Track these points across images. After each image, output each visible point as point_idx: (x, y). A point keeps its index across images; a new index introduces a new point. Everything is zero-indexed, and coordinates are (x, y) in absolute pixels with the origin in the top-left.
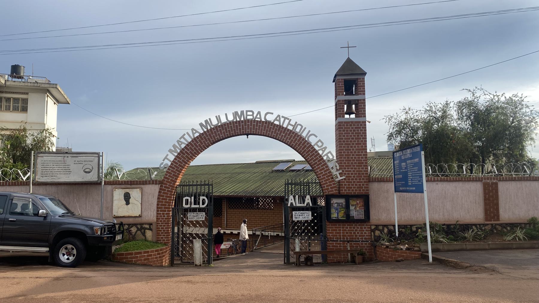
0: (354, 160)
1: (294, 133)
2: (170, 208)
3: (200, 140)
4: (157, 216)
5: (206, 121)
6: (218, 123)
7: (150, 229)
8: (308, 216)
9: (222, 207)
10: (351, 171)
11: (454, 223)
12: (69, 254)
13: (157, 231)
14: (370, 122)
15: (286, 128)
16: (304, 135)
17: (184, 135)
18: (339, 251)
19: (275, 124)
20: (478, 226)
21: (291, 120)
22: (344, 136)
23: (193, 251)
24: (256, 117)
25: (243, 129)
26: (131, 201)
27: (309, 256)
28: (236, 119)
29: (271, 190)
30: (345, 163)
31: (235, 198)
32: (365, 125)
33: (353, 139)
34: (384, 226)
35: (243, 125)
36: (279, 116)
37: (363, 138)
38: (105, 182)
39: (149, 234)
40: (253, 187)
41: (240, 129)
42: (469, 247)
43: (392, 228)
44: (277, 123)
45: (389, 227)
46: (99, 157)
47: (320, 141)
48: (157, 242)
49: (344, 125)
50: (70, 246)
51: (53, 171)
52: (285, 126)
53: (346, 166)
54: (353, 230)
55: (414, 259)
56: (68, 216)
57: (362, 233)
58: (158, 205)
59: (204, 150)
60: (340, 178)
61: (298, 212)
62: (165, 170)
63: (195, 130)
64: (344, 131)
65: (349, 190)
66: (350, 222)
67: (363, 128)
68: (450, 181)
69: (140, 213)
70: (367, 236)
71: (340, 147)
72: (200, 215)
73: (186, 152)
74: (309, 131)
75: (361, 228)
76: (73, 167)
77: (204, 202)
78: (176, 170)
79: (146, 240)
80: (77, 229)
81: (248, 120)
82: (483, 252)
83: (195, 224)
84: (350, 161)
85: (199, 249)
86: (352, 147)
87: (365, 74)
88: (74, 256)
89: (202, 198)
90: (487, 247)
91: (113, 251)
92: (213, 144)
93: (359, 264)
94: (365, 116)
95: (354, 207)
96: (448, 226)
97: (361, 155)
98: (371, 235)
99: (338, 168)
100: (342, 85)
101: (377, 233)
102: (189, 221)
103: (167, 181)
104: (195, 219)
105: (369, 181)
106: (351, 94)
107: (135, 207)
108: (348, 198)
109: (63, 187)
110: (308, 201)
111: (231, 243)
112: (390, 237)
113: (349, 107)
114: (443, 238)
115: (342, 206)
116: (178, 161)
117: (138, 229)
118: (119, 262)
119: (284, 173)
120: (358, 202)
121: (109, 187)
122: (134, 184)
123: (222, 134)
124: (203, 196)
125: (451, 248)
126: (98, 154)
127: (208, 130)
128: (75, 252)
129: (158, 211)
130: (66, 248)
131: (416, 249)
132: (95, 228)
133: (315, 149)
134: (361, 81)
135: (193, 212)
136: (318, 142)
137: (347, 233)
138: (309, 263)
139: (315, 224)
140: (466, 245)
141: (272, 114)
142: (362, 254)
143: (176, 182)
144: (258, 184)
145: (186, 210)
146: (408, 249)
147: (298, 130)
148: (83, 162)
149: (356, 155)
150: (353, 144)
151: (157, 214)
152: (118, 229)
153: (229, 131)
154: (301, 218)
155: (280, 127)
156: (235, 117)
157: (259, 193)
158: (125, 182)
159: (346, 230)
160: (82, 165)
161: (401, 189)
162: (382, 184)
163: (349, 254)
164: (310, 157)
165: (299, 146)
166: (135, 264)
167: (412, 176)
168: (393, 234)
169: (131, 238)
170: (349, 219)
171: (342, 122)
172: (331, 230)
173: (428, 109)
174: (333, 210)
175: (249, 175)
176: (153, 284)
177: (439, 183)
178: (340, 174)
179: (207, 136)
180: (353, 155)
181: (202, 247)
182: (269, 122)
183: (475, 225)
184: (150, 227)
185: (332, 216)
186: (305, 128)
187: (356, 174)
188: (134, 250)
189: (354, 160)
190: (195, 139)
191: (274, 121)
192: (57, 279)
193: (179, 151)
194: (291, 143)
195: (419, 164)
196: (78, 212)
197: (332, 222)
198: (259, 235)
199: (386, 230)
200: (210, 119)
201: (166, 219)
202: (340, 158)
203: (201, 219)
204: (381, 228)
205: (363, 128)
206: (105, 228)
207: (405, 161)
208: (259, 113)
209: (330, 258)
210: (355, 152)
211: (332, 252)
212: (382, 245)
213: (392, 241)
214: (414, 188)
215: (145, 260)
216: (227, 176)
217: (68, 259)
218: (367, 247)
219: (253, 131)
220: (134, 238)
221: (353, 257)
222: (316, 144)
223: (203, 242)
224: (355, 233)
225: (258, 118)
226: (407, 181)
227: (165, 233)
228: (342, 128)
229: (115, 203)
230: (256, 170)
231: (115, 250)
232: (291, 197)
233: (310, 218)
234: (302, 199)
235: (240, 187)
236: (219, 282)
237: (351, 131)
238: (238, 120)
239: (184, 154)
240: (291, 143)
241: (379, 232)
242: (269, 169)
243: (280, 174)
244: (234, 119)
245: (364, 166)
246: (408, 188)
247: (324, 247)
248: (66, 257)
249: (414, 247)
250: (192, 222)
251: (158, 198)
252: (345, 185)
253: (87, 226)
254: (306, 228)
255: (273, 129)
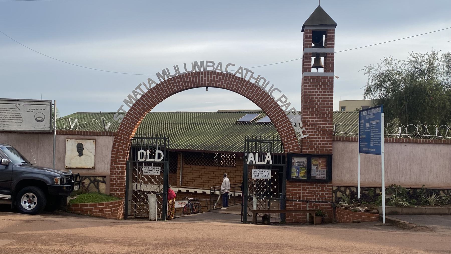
0: (318, 118)
1: (256, 87)
2: (124, 161)
3: (156, 91)
4: (111, 169)
5: (164, 71)
6: (176, 74)
7: (104, 182)
8: (267, 174)
9: (177, 161)
10: (314, 129)
11: (420, 187)
12: (30, 202)
13: (111, 184)
14: (338, 78)
15: (248, 81)
16: (267, 89)
17: (140, 85)
18: (297, 211)
19: (236, 77)
20: (446, 191)
21: (253, 73)
22: (309, 92)
23: (147, 206)
24: (217, 69)
25: (202, 81)
26: (84, 152)
27: (266, 215)
28: (196, 70)
29: (233, 145)
30: (309, 121)
31: (192, 152)
32: (333, 81)
33: (318, 95)
34: (347, 187)
35: (202, 77)
36: (241, 68)
37: (329, 95)
38: (57, 131)
39: (102, 187)
40: (213, 141)
41: (199, 80)
42: (428, 211)
43: (354, 189)
44: (238, 75)
45: (351, 188)
46: (51, 106)
47: (283, 96)
48: (110, 195)
49: (310, 80)
50: (31, 194)
51: (5, 119)
52: (247, 79)
53: (310, 124)
54: (314, 191)
55: (372, 221)
56: (26, 165)
57: (322, 194)
58: (112, 157)
59: (160, 102)
60: (303, 136)
61: (257, 170)
62: (120, 122)
63: (152, 80)
64: (309, 86)
65: (311, 149)
66: (311, 182)
67: (330, 83)
68: (420, 143)
69: (93, 166)
70: (328, 197)
71: (304, 103)
72: (156, 169)
73: (142, 103)
74: (273, 85)
75: (322, 189)
76: (25, 115)
77: (160, 156)
78: (131, 122)
79: (99, 193)
80: (37, 178)
81: (208, 72)
82: (439, 216)
83: (150, 180)
84: (315, 118)
85: (154, 204)
86: (317, 104)
87: (335, 25)
88: (35, 204)
89: (157, 152)
90: (447, 212)
91: (68, 202)
92: (169, 96)
93: (316, 224)
94: (333, 71)
95: (316, 167)
96: (415, 190)
97: (326, 113)
98: (332, 196)
99: (301, 125)
100: (310, 36)
101: (339, 194)
102: (145, 176)
103: (121, 133)
104: (150, 174)
105: (333, 141)
106: (321, 46)
107: (89, 158)
108: (310, 157)
109: (13, 136)
110: (268, 159)
111: (187, 202)
112: (351, 199)
113: (317, 61)
114: (404, 201)
115: (303, 165)
116: (134, 112)
117: (91, 182)
118: (74, 213)
119: (250, 126)
120: (320, 162)
121: (62, 137)
122: (88, 135)
123: (179, 86)
124: (159, 149)
125: (409, 211)
126: (50, 102)
127: (165, 81)
128: (36, 200)
129: (112, 163)
130: (27, 196)
131: (374, 211)
132: (55, 178)
133: (278, 105)
134: (330, 33)
135: (149, 166)
136: (281, 97)
137: (307, 193)
138: (266, 222)
139: (275, 183)
140: (425, 209)
141: (234, 65)
142: (322, 215)
143: (131, 134)
144: (218, 138)
145: (141, 164)
146: (366, 211)
147: (261, 84)
148: (35, 111)
149: (321, 113)
150: (319, 101)
151: (111, 166)
152: (75, 179)
153: (188, 82)
154: (260, 177)
155: (242, 80)
156: (194, 68)
157: (219, 147)
158: (78, 132)
159: (306, 190)
160: (34, 114)
161: (364, 149)
162: (347, 144)
163: (308, 214)
164: (273, 113)
165: (261, 101)
166: (90, 216)
167: (374, 137)
168: (356, 196)
169: (84, 191)
170: (309, 179)
171: (308, 77)
172: (291, 190)
173: (413, 59)
174: (294, 170)
175: (209, 126)
176: (117, 228)
177: (407, 144)
178: (303, 132)
179: (164, 87)
180: (318, 112)
181: (158, 203)
182: (231, 74)
183: (443, 190)
184: (103, 180)
185: (292, 175)
186: (269, 82)
187: (320, 132)
188: (89, 202)
189: (318, 118)
190: (151, 89)
191: (236, 73)
192: (28, 221)
193: (134, 102)
194: (253, 97)
195: (379, 126)
196: (35, 162)
197: (293, 182)
198: (218, 195)
199: (348, 192)
200: (167, 69)
201: (120, 172)
202: (304, 115)
203: (156, 174)
204: (343, 189)
205: (330, 83)
206: (63, 178)
207: (369, 121)
208: (220, 64)
209: (289, 217)
210: (320, 110)
211: (290, 211)
212: (342, 206)
213: (352, 203)
214: (374, 150)
215: (100, 212)
216: (183, 126)
217: (29, 206)
218: (327, 208)
219: (213, 84)
220: (87, 190)
221: (311, 217)
222: (280, 99)
223: (158, 197)
224: (315, 193)
225: (219, 70)
226: (369, 144)
227: (119, 186)
228: (308, 83)
229: (68, 154)
230: (219, 121)
231: (70, 202)
232: (251, 155)
233: (270, 176)
234: (262, 156)
235: (197, 141)
236: (176, 229)
237: (317, 86)
238: (198, 71)
239: (140, 106)
240: (253, 97)
241: (341, 193)
242: (233, 121)
243: (245, 127)
244: (193, 70)
245: (329, 124)
246: (370, 150)
247: (284, 206)
248: (27, 204)
249: (373, 209)
250: (146, 176)
251: (112, 151)
252: (308, 143)
253: (47, 175)
254: (266, 187)
255: (234, 82)
